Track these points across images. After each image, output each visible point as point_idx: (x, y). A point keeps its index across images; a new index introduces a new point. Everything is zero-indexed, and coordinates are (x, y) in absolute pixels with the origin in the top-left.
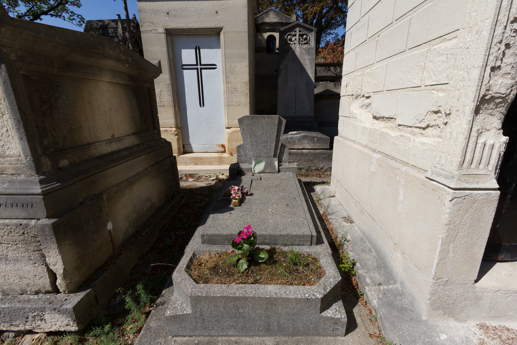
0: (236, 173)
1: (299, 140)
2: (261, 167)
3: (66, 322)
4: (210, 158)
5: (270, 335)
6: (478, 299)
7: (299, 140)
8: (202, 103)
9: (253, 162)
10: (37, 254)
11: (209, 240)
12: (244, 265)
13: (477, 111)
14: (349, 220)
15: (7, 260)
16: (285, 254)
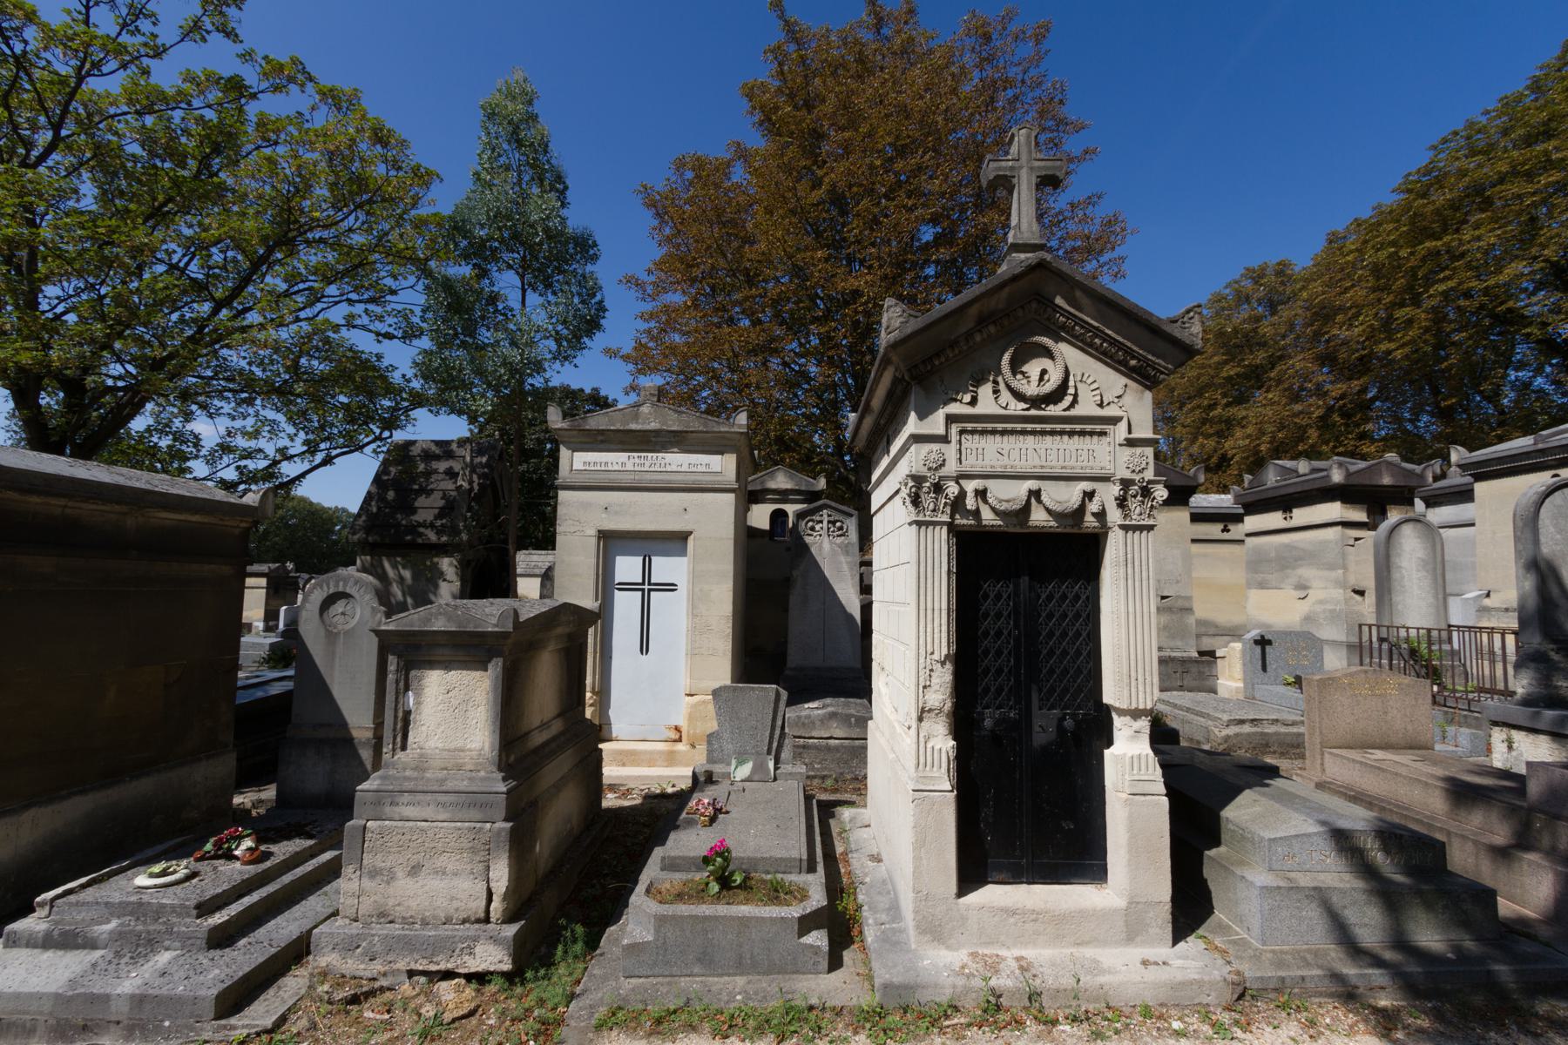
0: (703, 780)
1: (822, 721)
2: (745, 770)
3: (499, 957)
4: (651, 752)
5: (742, 974)
6: (964, 919)
7: (822, 721)
8: (644, 647)
9: (734, 762)
10: (481, 867)
11: (670, 865)
12: (715, 887)
13: (920, 719)
14: (877, 859)
15: (444, 873)
16: (764, 882)
